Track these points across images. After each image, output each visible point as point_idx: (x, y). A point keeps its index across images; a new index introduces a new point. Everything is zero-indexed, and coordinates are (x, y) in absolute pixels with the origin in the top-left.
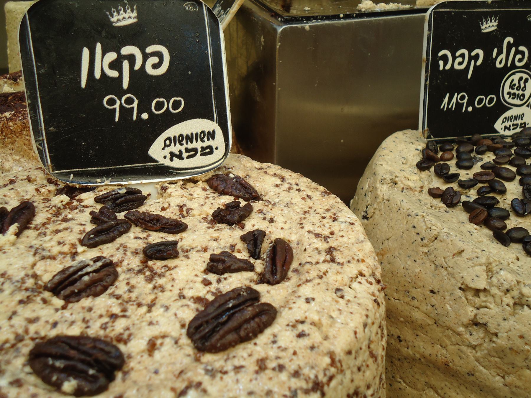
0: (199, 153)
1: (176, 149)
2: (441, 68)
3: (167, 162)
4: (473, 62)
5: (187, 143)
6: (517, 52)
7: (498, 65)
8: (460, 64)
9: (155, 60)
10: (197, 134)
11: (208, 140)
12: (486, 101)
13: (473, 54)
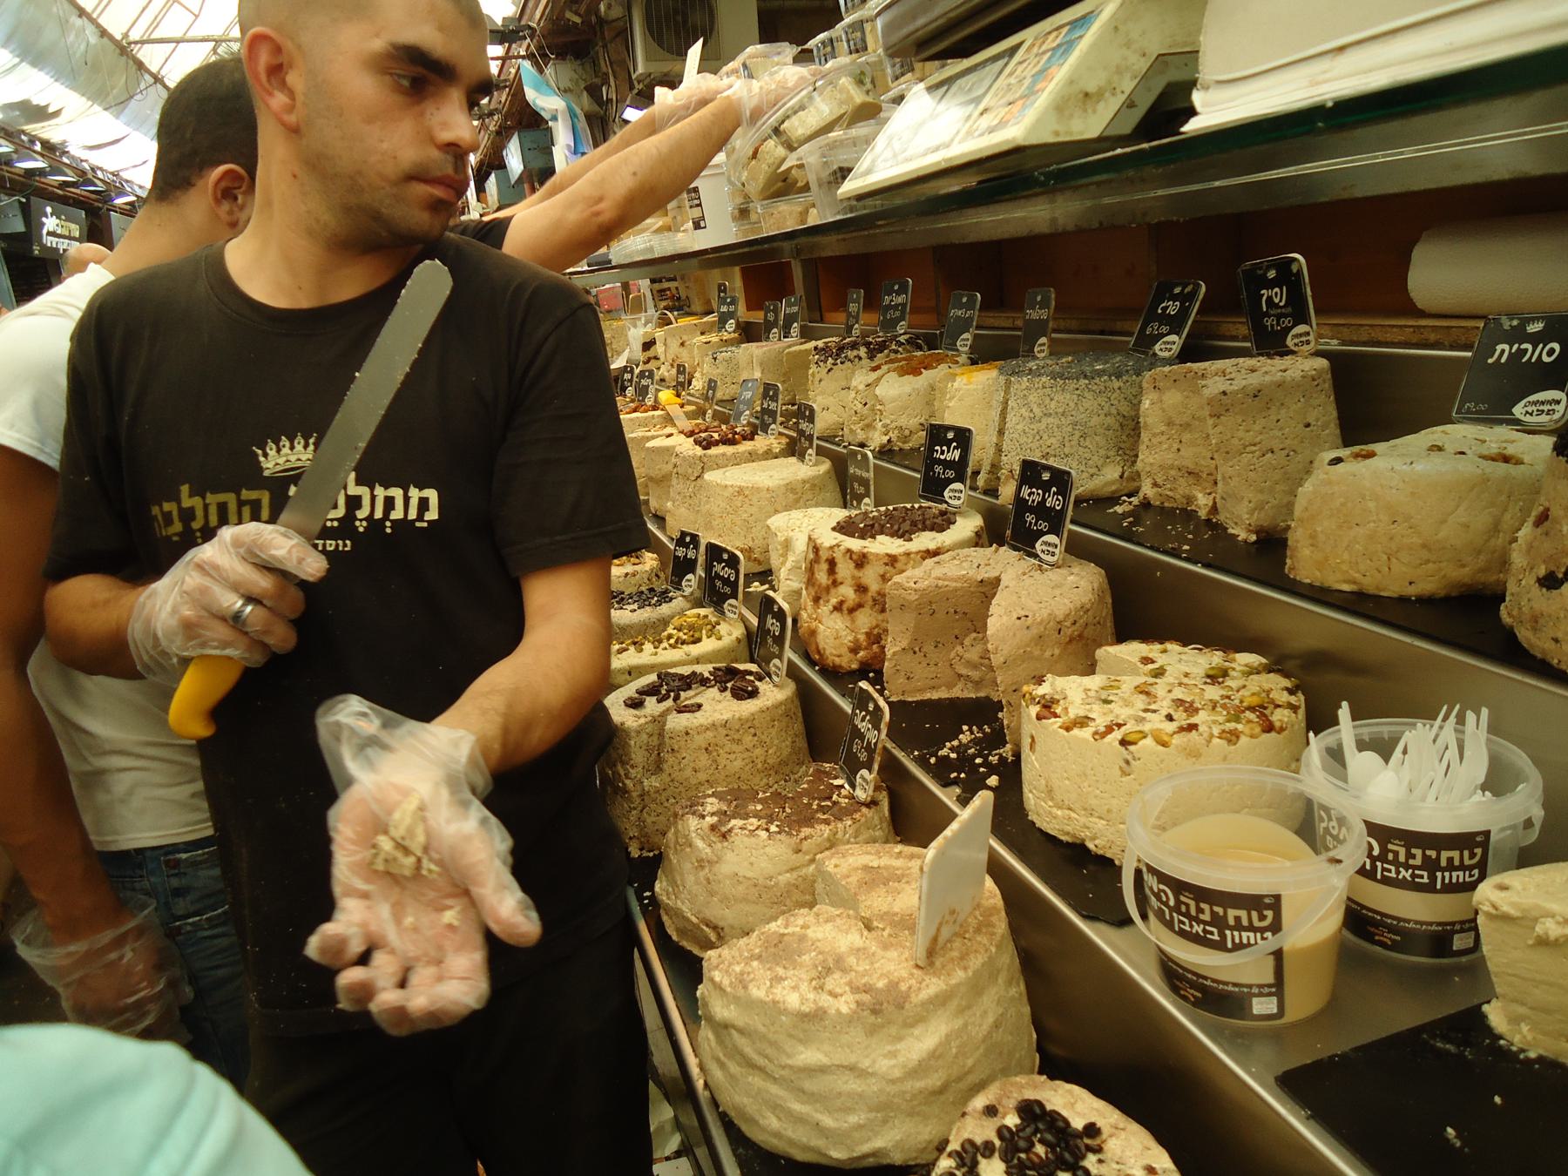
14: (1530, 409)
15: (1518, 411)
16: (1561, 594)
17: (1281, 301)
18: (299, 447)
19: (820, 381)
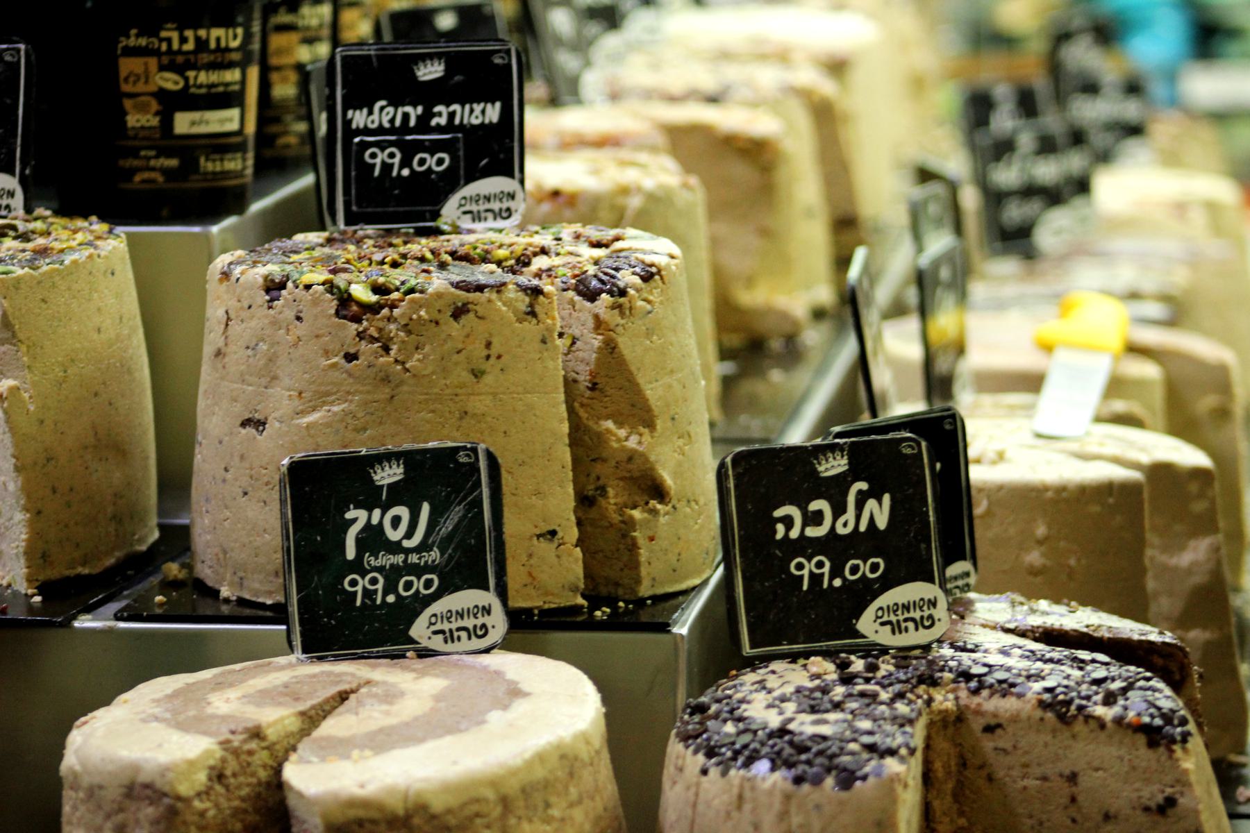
2: (780, 535)
11: (483, 616)
12: (865, 568)
16: (939, 620)
17: (409, 535)
18: (394, 466)
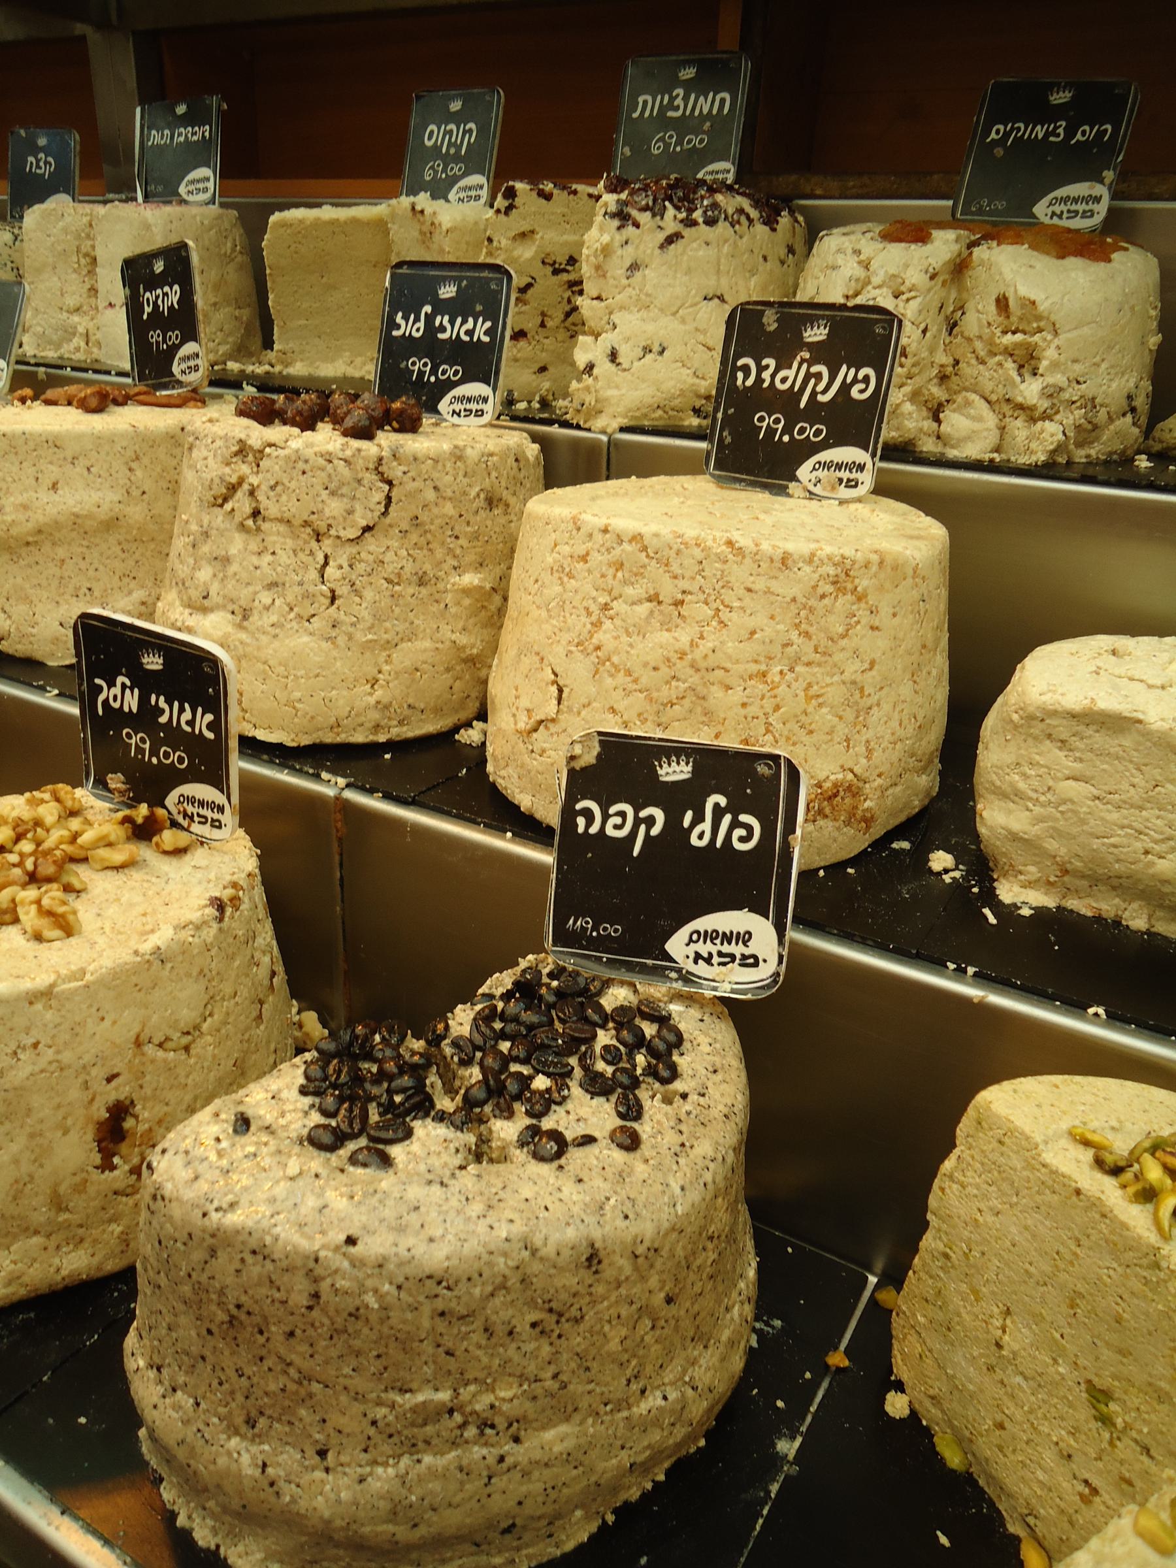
0: (737, 961)
1: (704, 948)
2: (581, 830)
3: (690, 966)
4: (643, 828)
5: (722, 944)
6: (735, 824)
7: (694, 841)
8: (617, 827)
9: (618, 820)
10: (739, 933)
13: (643, 814)
14: (1057, 209)
15: (1041, 210)
19: (634, 267)
